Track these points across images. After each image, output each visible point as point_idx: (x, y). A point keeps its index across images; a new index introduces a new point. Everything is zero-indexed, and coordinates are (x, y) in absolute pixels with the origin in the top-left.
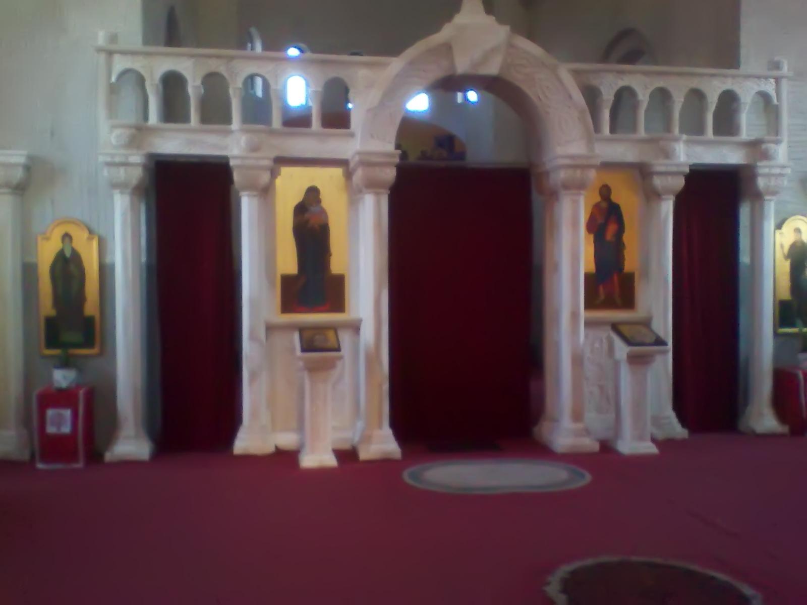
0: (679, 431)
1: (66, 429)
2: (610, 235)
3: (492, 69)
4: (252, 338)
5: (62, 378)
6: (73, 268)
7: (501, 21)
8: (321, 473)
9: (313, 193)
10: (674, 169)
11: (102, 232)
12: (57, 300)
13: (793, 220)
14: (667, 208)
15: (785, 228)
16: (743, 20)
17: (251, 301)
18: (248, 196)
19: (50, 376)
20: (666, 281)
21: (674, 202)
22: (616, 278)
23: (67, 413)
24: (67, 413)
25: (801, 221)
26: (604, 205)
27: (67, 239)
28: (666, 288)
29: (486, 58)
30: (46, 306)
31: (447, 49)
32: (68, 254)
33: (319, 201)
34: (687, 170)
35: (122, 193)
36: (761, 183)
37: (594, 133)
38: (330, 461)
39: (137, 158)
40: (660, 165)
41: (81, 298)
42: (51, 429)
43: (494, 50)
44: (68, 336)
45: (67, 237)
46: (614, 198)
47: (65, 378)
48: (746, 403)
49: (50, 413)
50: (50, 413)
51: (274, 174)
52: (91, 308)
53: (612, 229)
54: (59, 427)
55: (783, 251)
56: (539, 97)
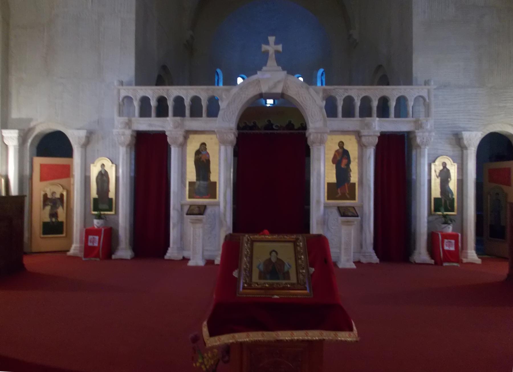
0: (375, 259)
1: (96, 244)
2: (343, 166)
3: (279, 90)
4: (174, 209)
5: (96, 223)
6: (105, 178)
7: (284, 69)
8: (196, 268)
9: (203, 144)
10: (372, 134)
11: (117, 164)
12: (98, 193)
13: (442, 158)
14: (371, 153)
15: (437, 163)
16: (414, 56)
17: (174, 192)
18: (174, 147)
19: (93, 222)
20: (369, 187)
21: (374, 150)
22: (346, 184)
23: (97, 238)
24: (97, 238)
25: (447, 159)
26: (341, 151)
27: (103, 166)
28: (370, 191)
29: (275, 86)
30: (94, 193)
31: (258, 81)
32: (103, 172)
33: (206, 149)
34: (379, 134)
35: (123, 147)
36: (418, 140)
37: (326, 117)
38: (201, 263)
39: (128, 133)
40: (364, 132)
41: (108, 191)
42: (90, 244)
43: (279, 82)
44: (101, 206)
45: (103, 165)
46: (345, 147)
47: (98, 223)
48: (415, 249)
49: (90, 237)
50: (90, 237)
51: (186, 138)
52: (112, 195)
53: (345, 161)
54: (93, 243)
55: (436, 175)
56: (302, 102)
